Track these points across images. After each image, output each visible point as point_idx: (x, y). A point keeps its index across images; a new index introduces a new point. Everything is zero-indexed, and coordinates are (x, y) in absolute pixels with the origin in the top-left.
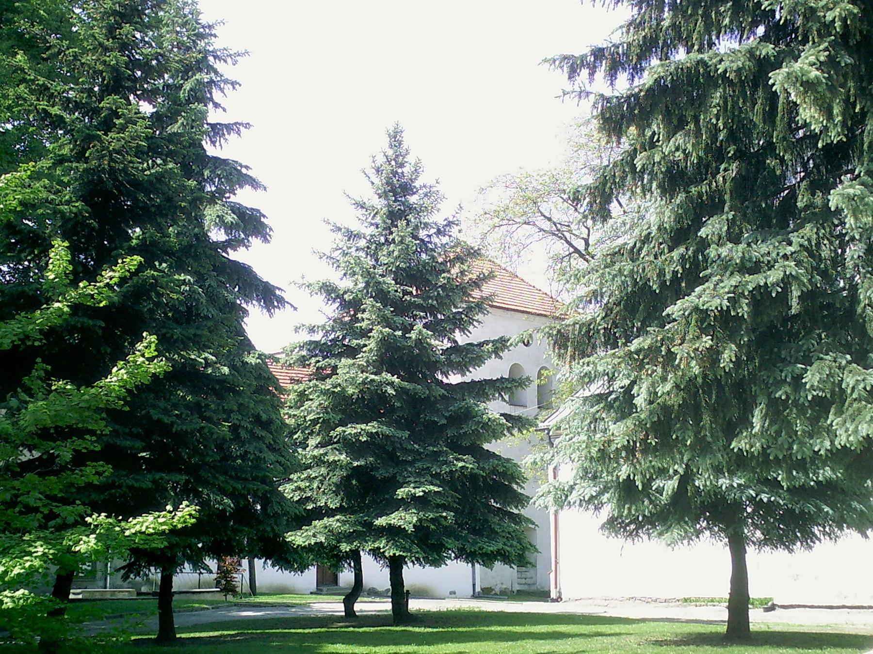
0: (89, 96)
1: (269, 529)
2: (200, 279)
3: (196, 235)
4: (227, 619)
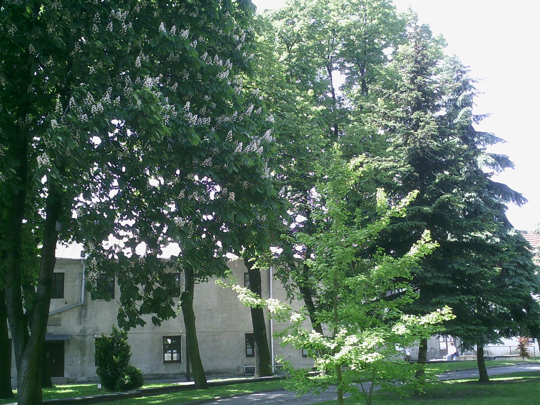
0: (407, 114)
1: (531, 321)
2: (480, 194)
3: (475, 171)
4: (523, 371)
